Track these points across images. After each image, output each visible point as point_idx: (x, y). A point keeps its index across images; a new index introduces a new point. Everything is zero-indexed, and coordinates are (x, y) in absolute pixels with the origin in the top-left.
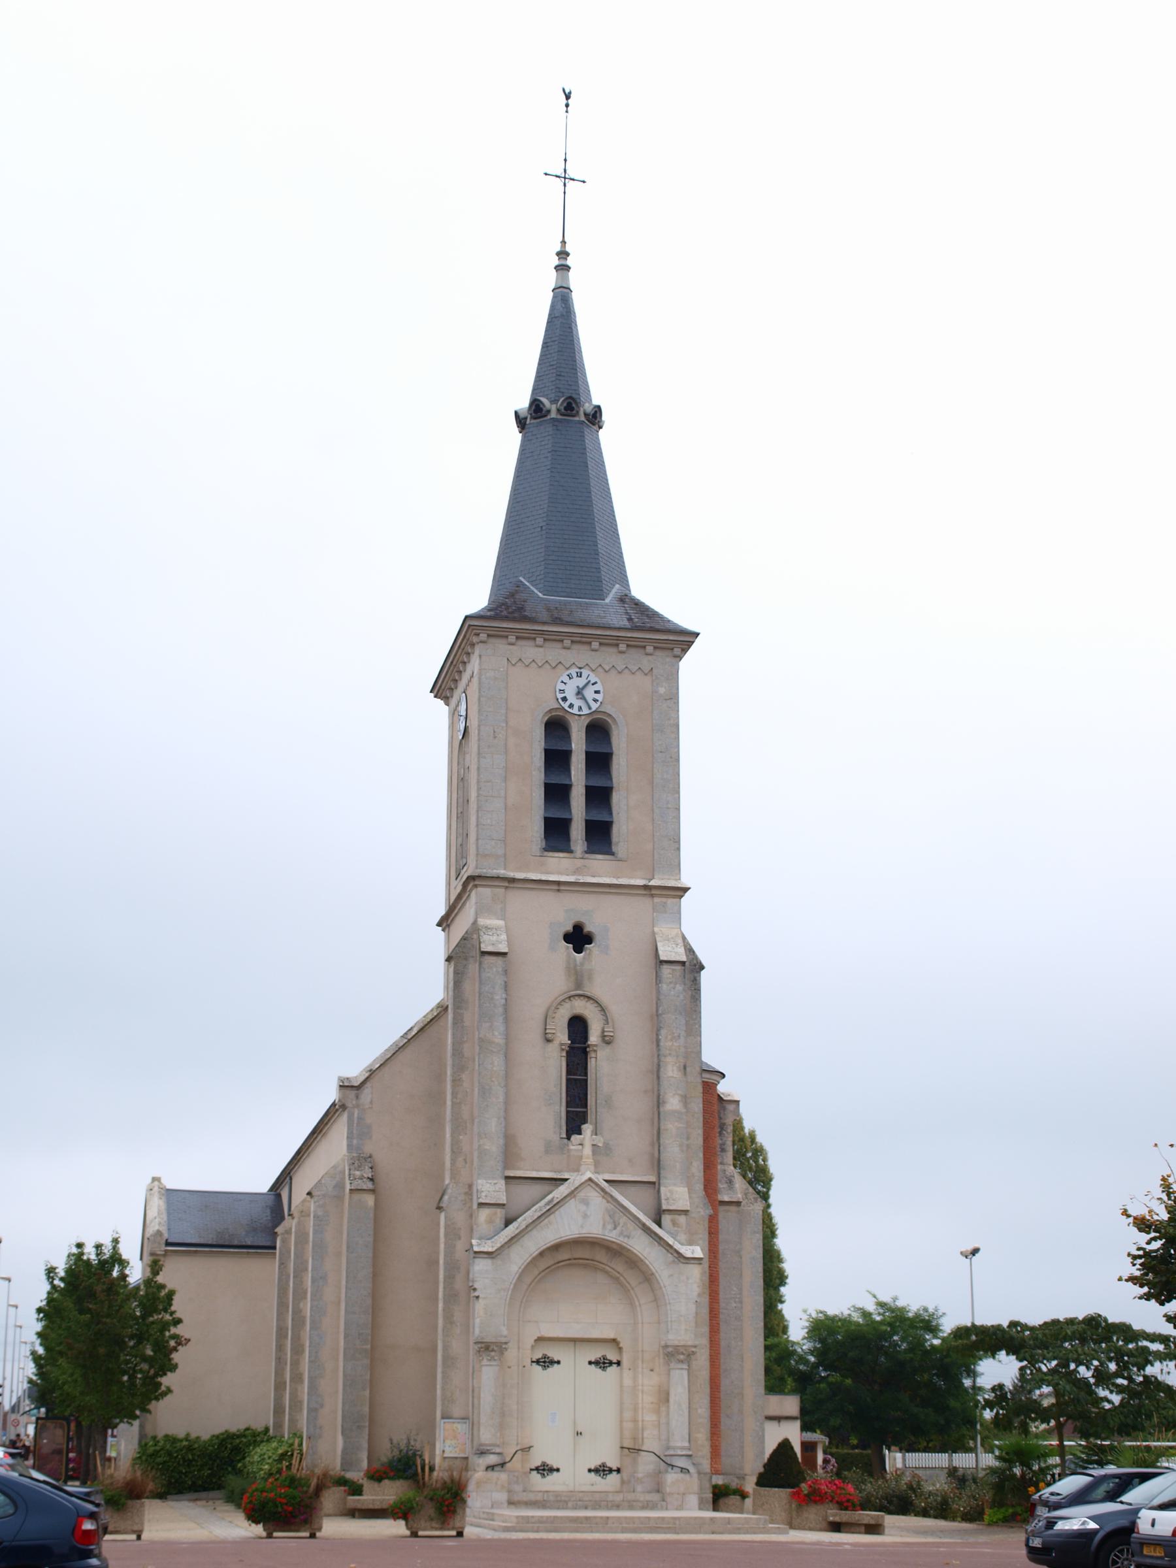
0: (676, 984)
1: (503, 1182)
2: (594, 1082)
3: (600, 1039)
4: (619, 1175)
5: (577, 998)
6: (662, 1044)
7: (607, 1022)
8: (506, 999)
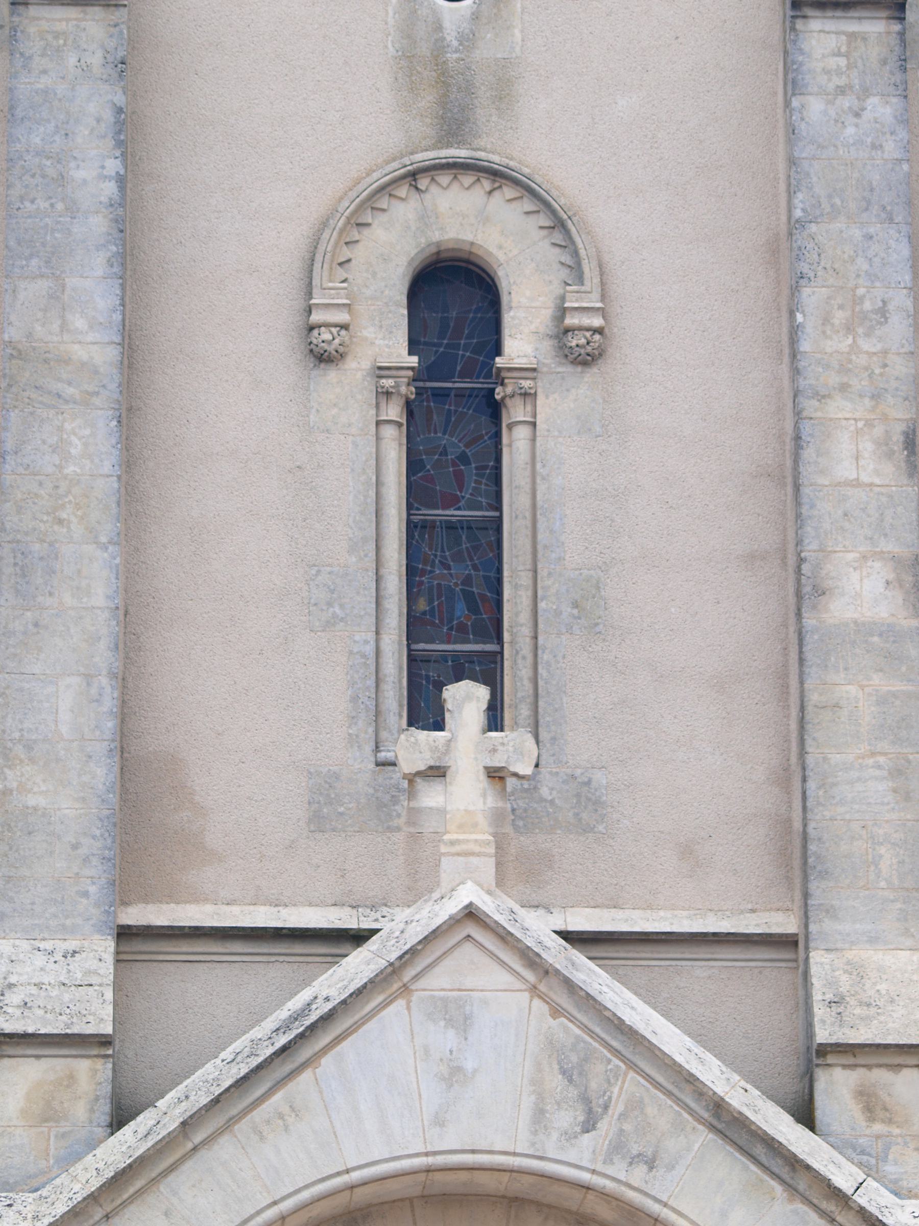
0: (866, 92)
1: (107, 946)
2: (524, 523)
3: (547, 346)
4: (636, 914)
5: (444, 179)
6: (805, 346)
7: (576, 271)
8: (121, 181)
